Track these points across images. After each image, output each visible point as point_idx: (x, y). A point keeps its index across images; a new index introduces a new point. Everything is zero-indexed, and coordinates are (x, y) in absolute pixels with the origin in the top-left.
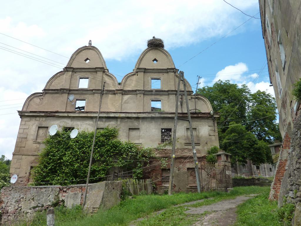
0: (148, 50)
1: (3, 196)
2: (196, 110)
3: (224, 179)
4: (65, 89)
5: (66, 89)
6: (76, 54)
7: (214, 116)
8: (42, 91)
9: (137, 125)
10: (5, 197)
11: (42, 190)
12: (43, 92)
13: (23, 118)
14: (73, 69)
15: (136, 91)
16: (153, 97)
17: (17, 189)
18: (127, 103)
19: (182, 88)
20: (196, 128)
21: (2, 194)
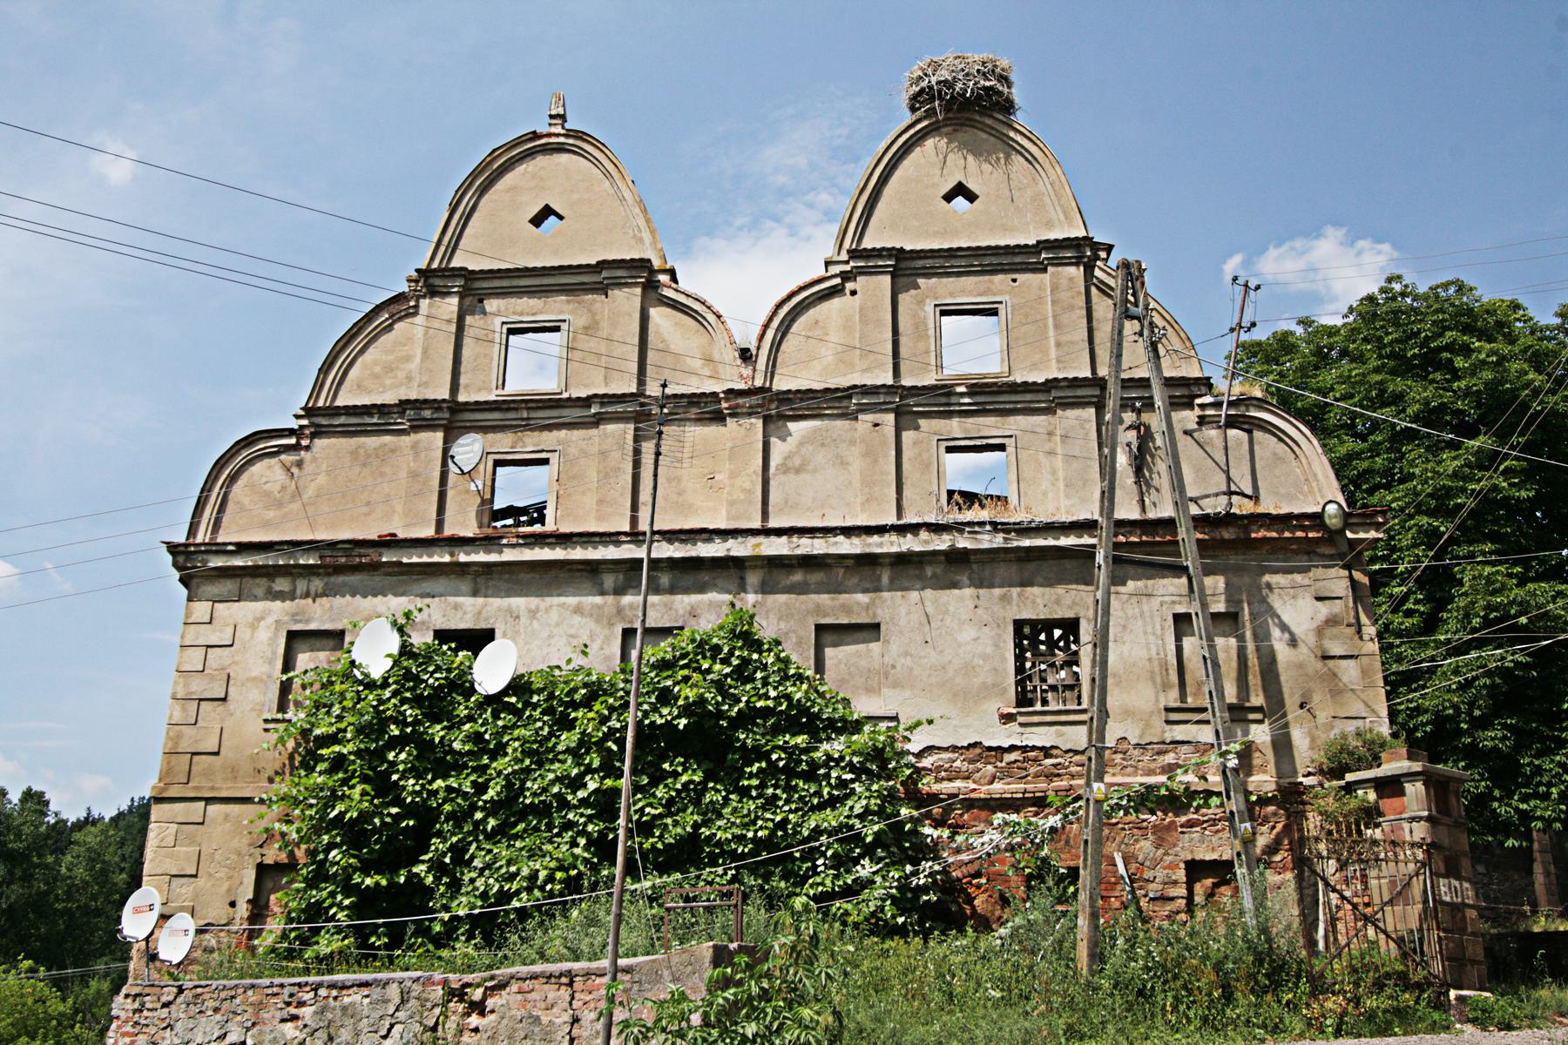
11: (347, 1000)
14: (467, 279)
16: (956, 427)
17: (205, 996)
18: (798, 471)
19: (1136, 363)
21: (119, 1027)
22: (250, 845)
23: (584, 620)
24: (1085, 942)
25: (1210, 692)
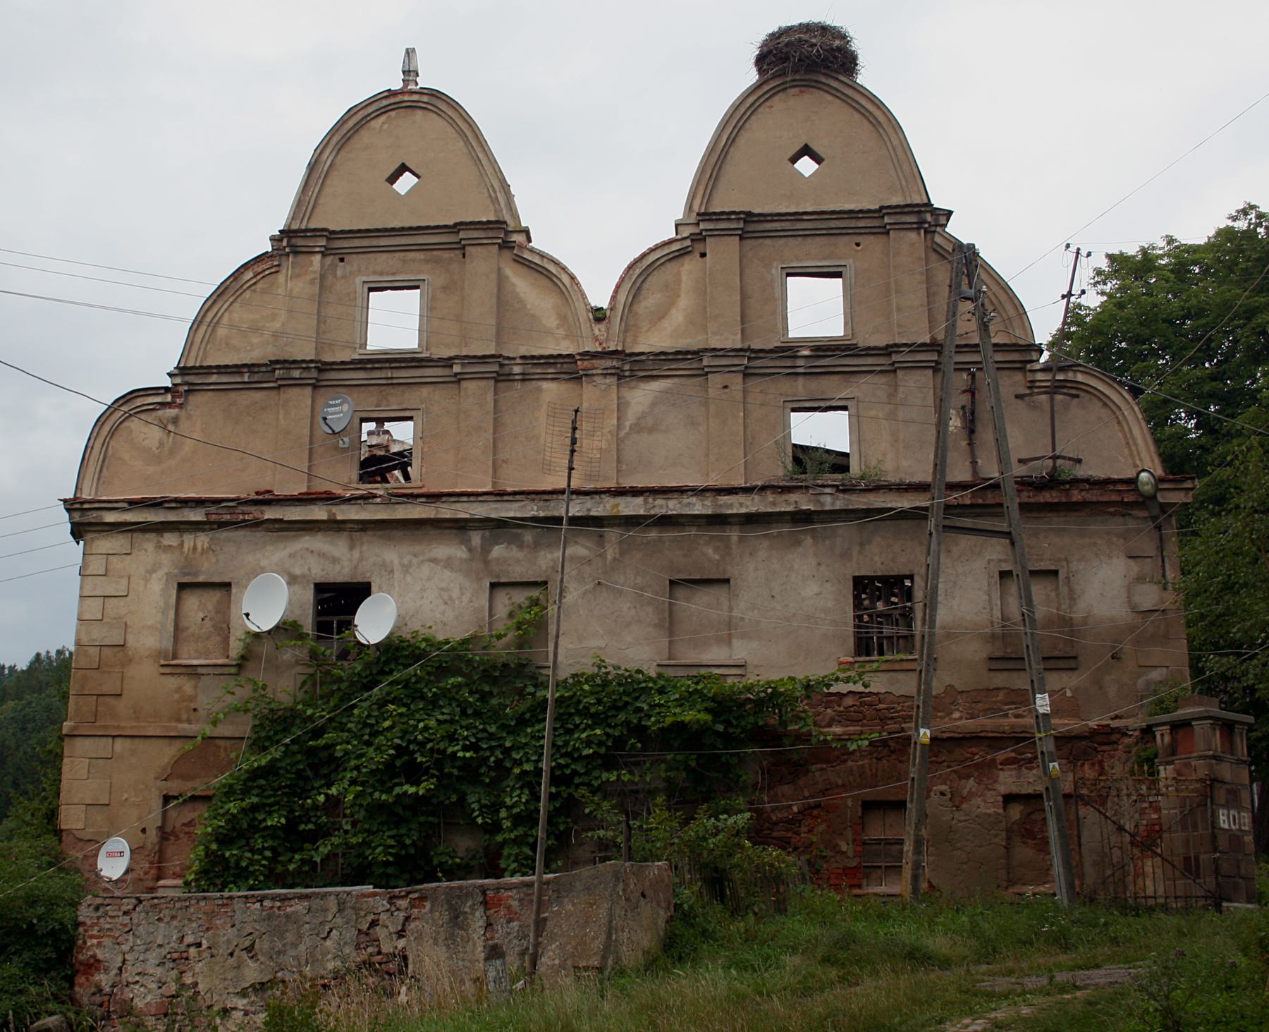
0: (760, 92)
1: (92, 937)
2: (1059, 462)
3: (1206, 856)
4: (295, 362)
5: (303, 361)
6: (335, 139)
7: (1161, 498)
8: (170, 375)
9: (717, 557)
10: (106, 941)
12: (174, 385)
13: (93, 540)
14: (328, 239)
15: (697, 354)
16: (801, 387)
18: (651, 430)
19: (967, 327)
20: (1055, 573)
22: (156, 778)
23: (454, 575)
24: (910, 864)
25: (1027, 646)
